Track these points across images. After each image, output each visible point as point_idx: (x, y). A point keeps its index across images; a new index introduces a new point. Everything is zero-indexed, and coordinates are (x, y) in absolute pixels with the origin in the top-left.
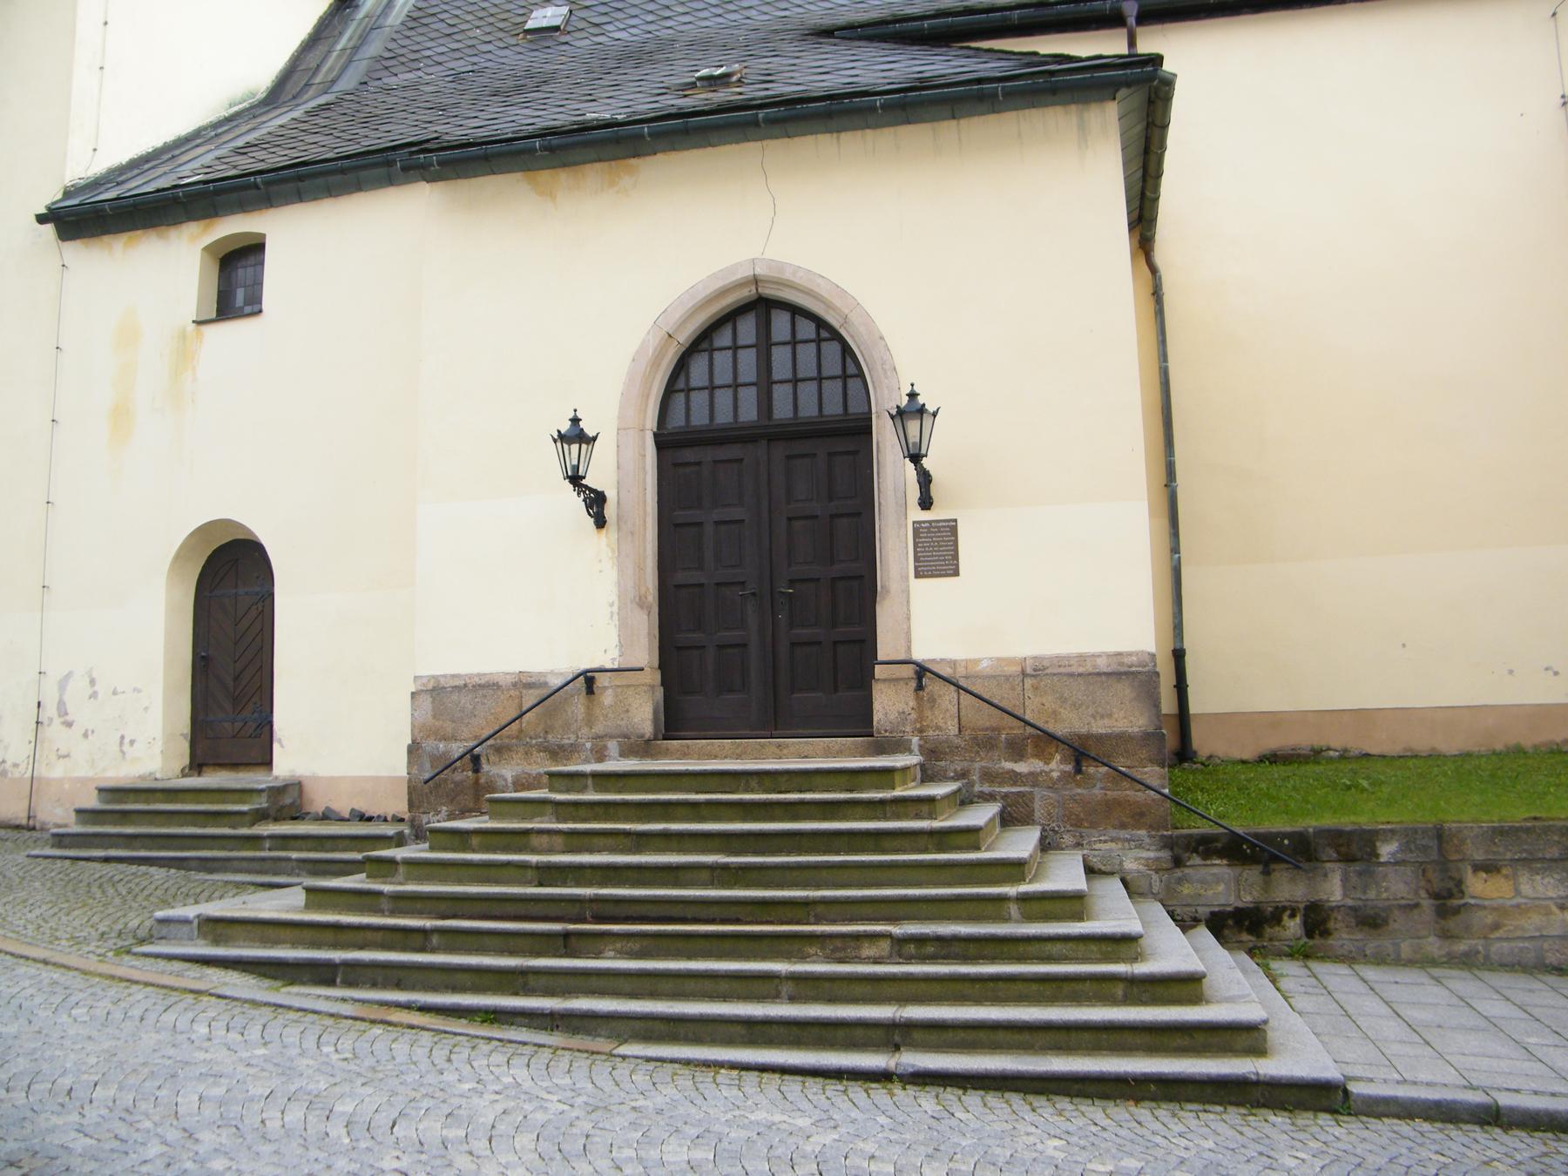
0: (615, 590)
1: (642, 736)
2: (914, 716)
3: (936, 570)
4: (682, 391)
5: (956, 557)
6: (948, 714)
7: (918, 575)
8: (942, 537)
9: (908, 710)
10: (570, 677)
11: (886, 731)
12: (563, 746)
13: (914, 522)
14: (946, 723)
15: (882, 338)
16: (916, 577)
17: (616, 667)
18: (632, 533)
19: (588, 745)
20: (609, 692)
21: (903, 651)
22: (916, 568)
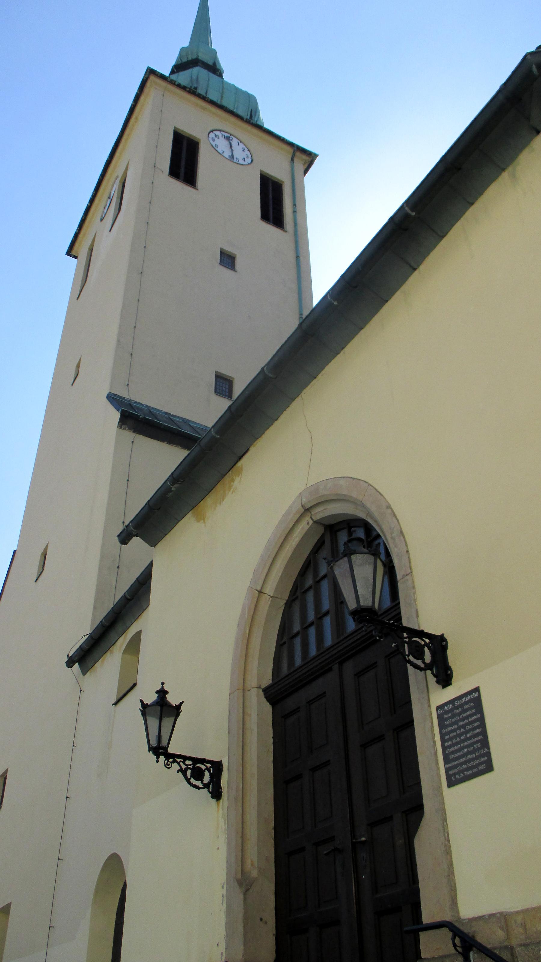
5: (485, 743)
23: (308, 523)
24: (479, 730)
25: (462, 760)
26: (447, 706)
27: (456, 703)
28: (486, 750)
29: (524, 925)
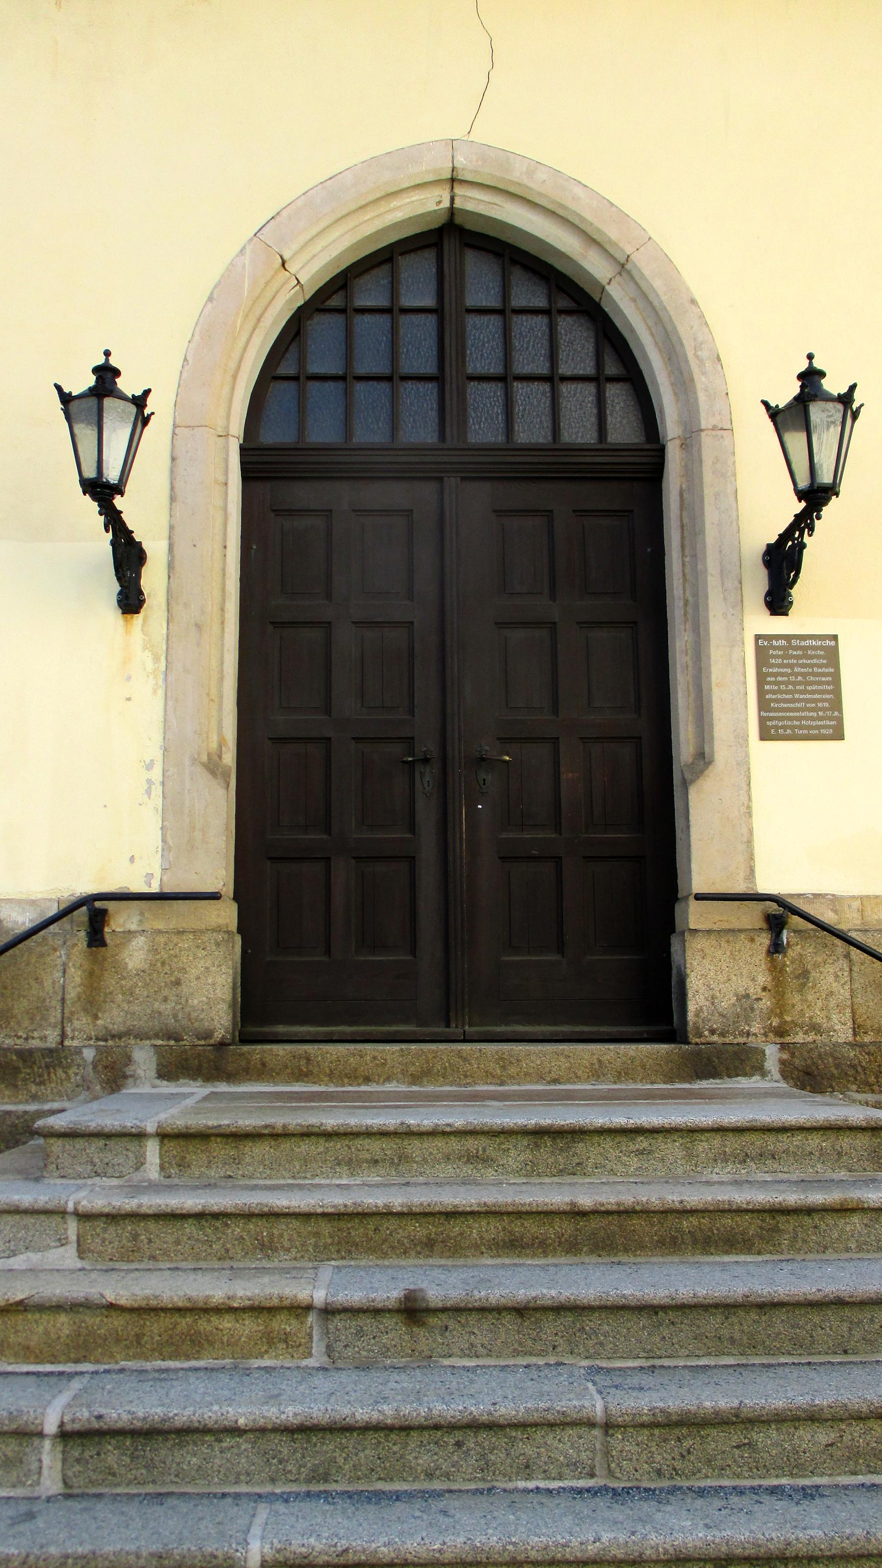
0: (157, 738)
1: (208, 1035)
2: (766, 1003)
3: (801, 727)
4: (505, 295)
5: (837, 704)
6: (832, 1003)
7: (765, 735)
8: (812, 666)
9: (754, 990)
10: (53, 911)
11: (713, 1032)
12: (31, 1052)
13: (758, 637)
14: (829, 1018)
15: (693, 302)
16: (763, 738)
17: (155, 888)
18: (198, 627)
19: (89, 1054)
20: (140, 941)
21: (742, 875)
22: (762, 721)
23: (440, 202)
24: (830, 688)
25: (796, 714)
26: (777, 640)
27: (794, 642)
28: (836, 713)
29: (862, 912)
